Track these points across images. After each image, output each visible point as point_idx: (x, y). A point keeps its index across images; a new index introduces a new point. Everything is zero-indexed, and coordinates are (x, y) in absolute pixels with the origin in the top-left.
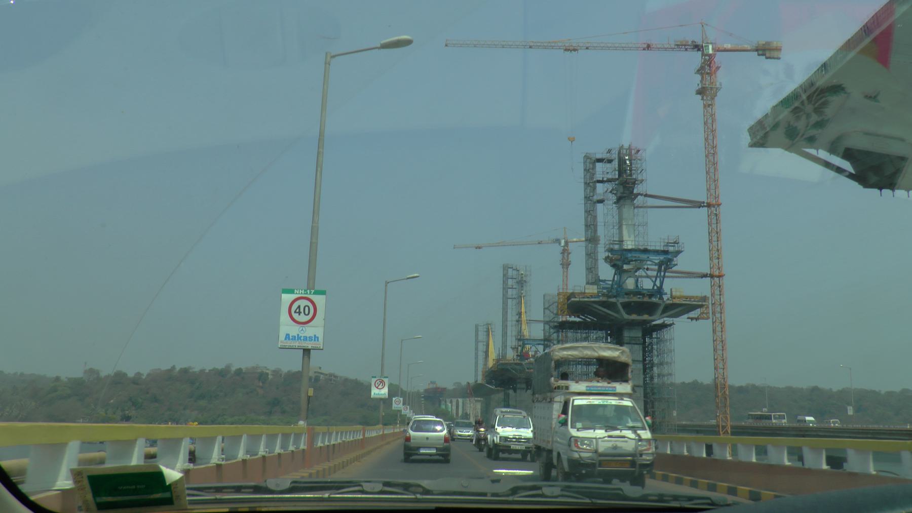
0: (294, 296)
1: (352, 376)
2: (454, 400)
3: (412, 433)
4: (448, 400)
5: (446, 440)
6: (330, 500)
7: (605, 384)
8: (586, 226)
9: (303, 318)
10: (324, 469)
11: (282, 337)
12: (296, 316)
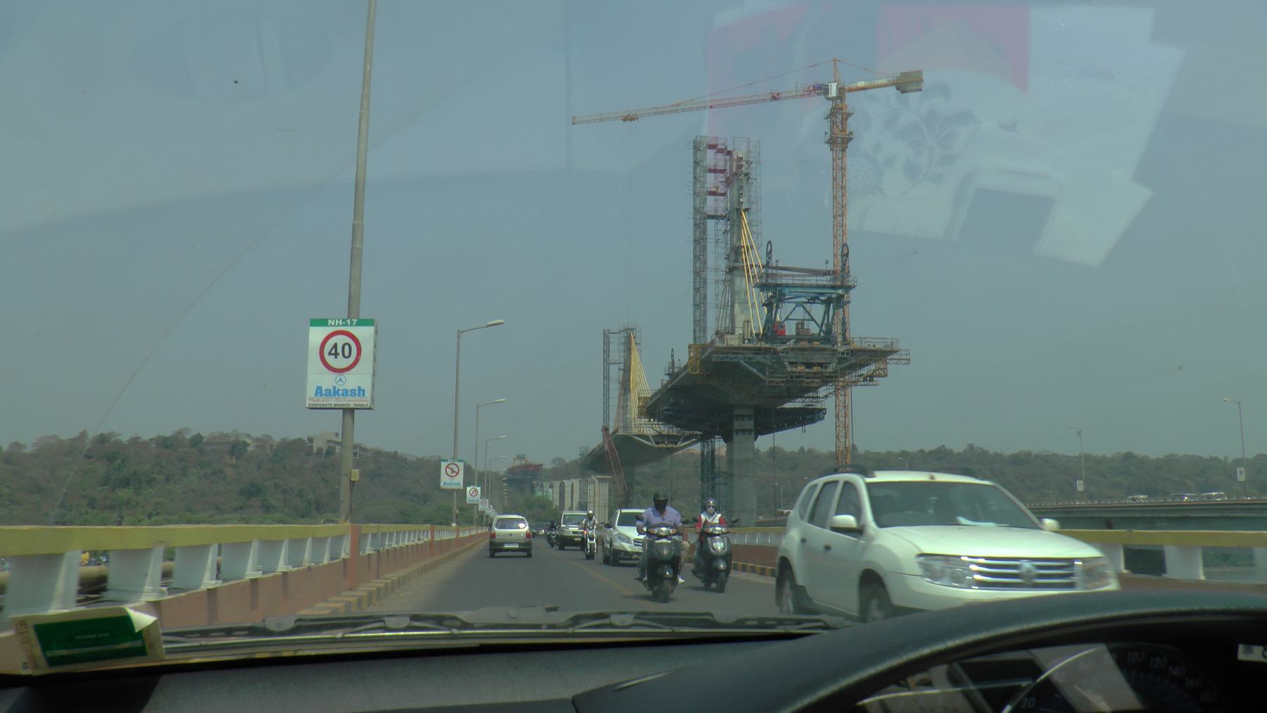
0: (330, 330)
1: (388, 448)
2: (557, 484)
3: (497, 530)
4: (546, 485)
5: (528, 535)
6: (344, 640)
8: (695, 305)
9: (341, 363)
10: (387, 585)
11: (311, 392)
12: (330, 360)
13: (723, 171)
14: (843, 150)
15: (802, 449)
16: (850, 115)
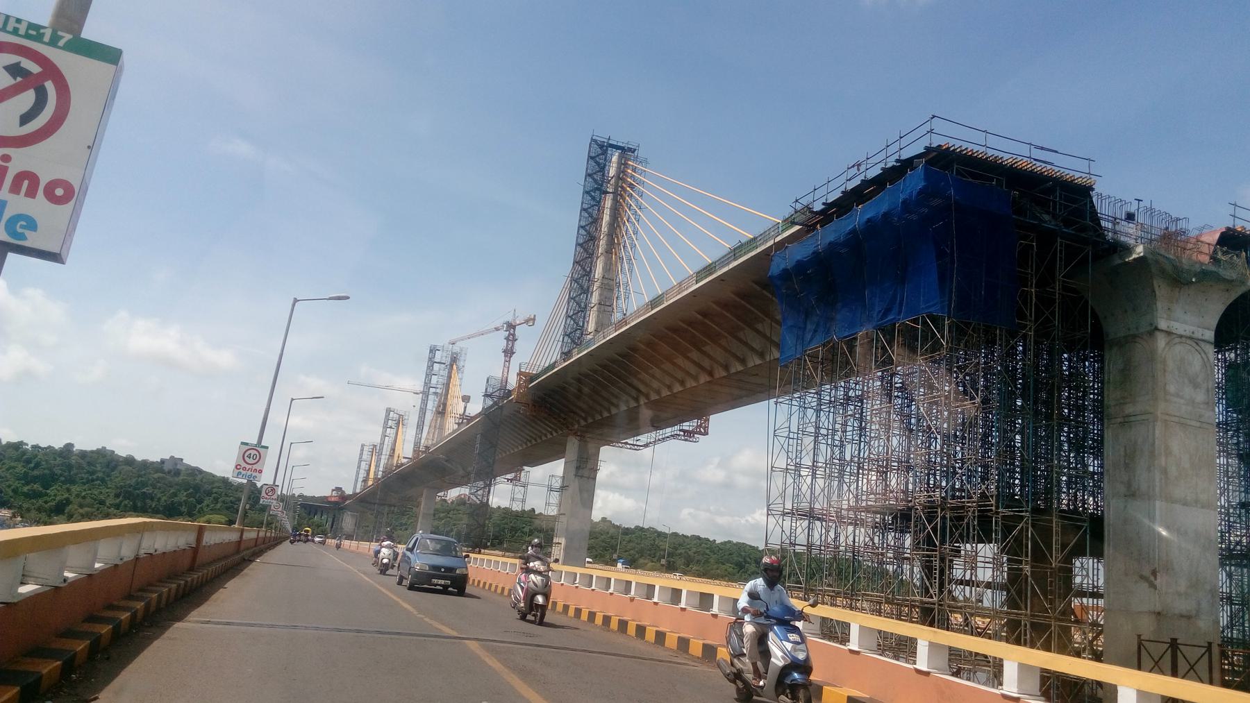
9: (251, 461)
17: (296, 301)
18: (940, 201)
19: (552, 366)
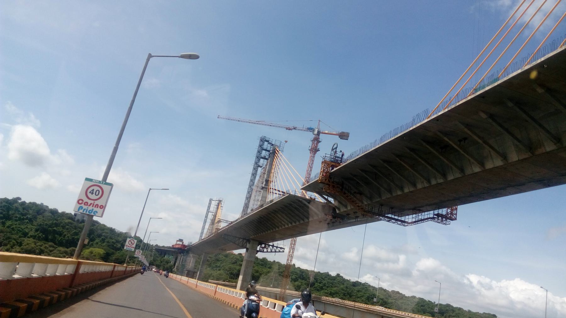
7: (340, 300)
9: (93, 197)
12: (89, 195)
13: (269, 151)
14: (314, 154)
15: (274, 261)
16: (320, 142)
17: (150, 56)
18: (38, 301)
19: (239, 219)
